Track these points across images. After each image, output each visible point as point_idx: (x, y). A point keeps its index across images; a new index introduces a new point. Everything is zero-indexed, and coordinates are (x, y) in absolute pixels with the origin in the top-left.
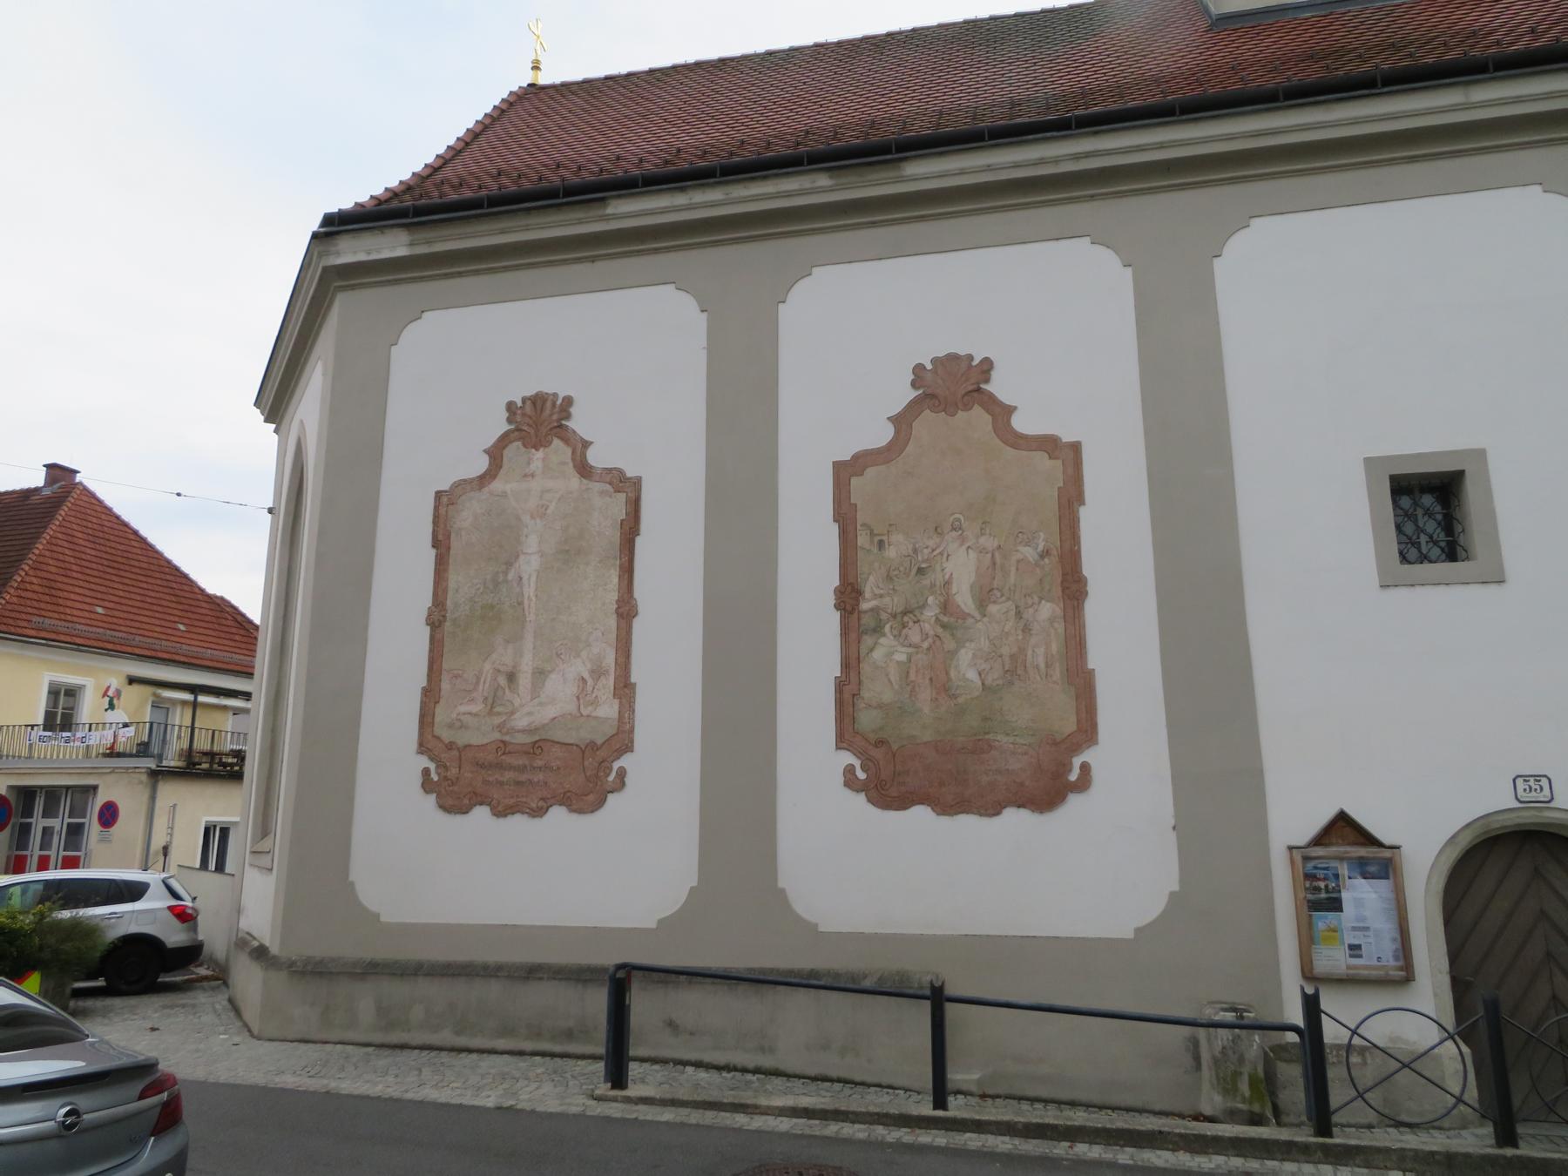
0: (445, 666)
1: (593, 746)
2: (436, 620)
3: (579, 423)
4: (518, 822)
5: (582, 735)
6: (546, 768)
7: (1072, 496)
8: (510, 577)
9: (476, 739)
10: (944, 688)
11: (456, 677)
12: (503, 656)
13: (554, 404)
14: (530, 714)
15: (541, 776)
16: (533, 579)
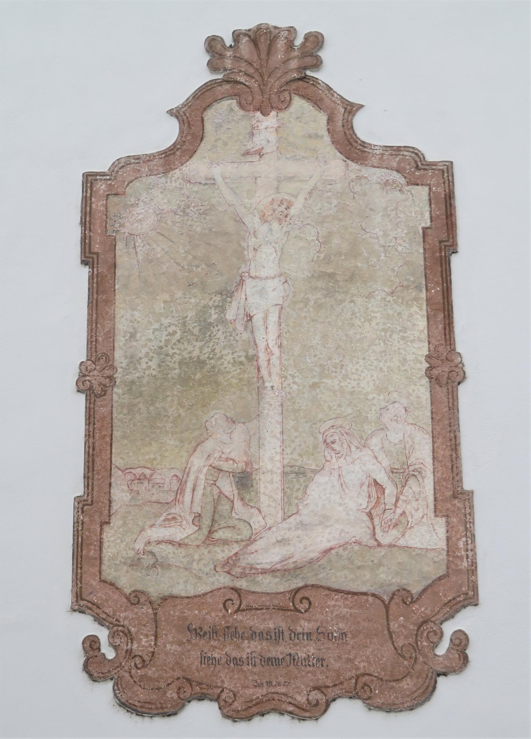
0: (117, 461)
1: (404, 597)
2: (96, 383)
3: (335, 73)
5: (384, 578)
6: (322, 634)
8: (230, 315)
9: (182, 586)
11: (141, 478)
12: (227, 445)
13: (290, 45)
14: (282, 542)
15: (308, 650)
16: (273, 318)
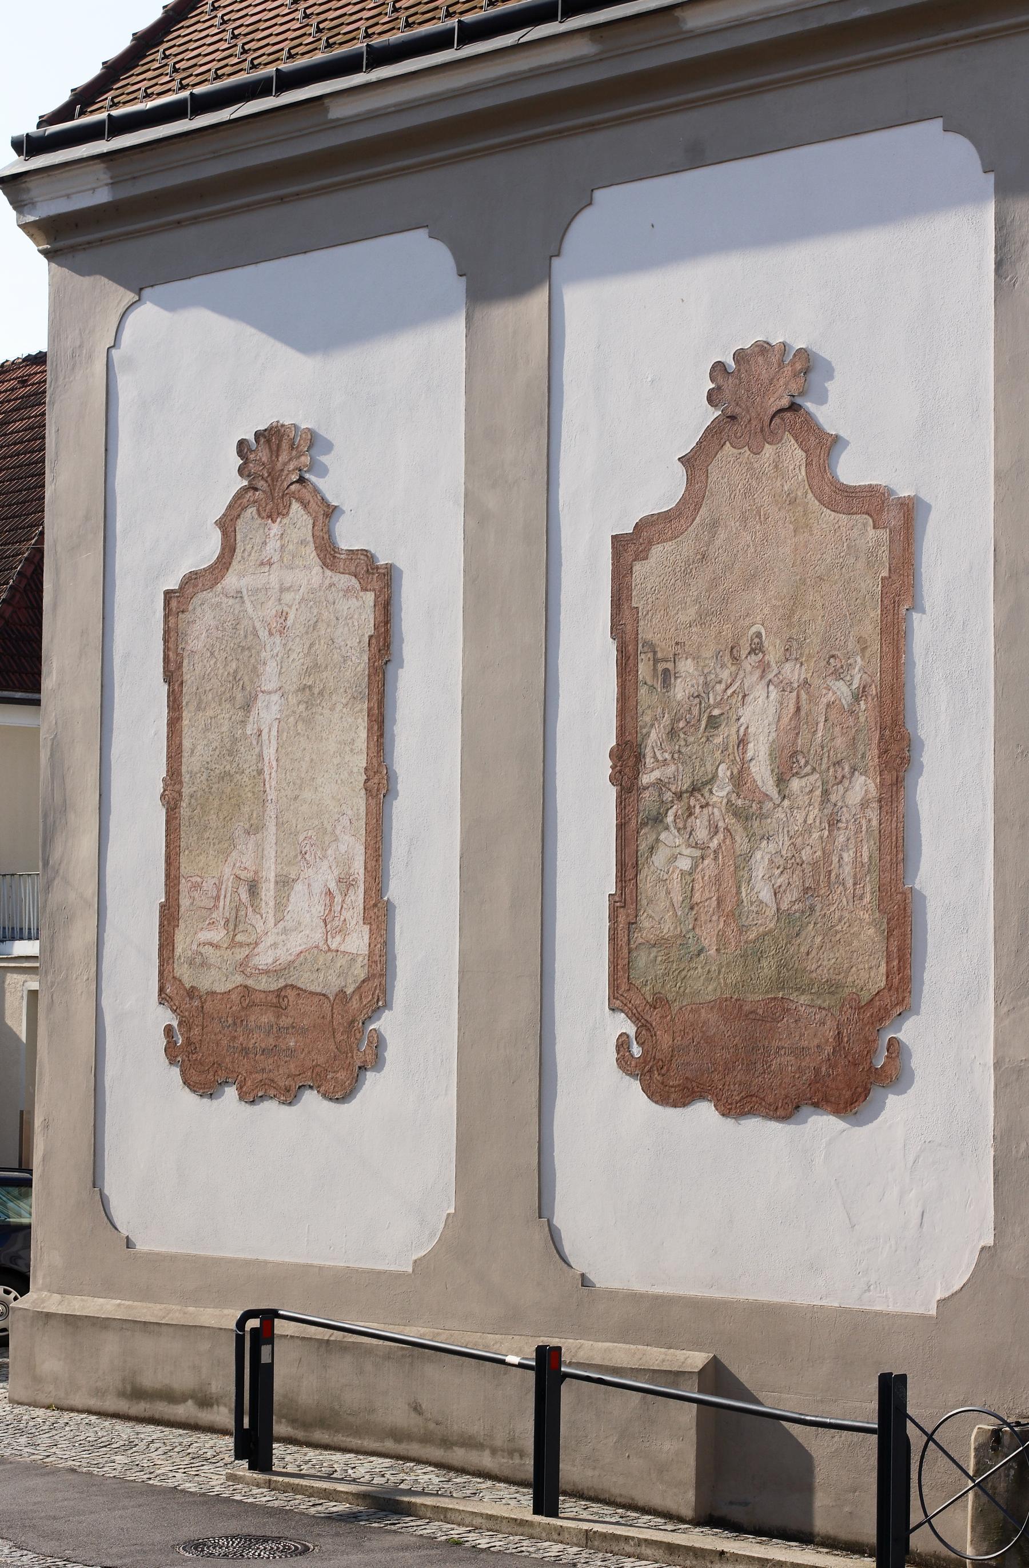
4: (270, 1108)
5: (327, 981)
7: (900, 588)
10: (732, 911)
